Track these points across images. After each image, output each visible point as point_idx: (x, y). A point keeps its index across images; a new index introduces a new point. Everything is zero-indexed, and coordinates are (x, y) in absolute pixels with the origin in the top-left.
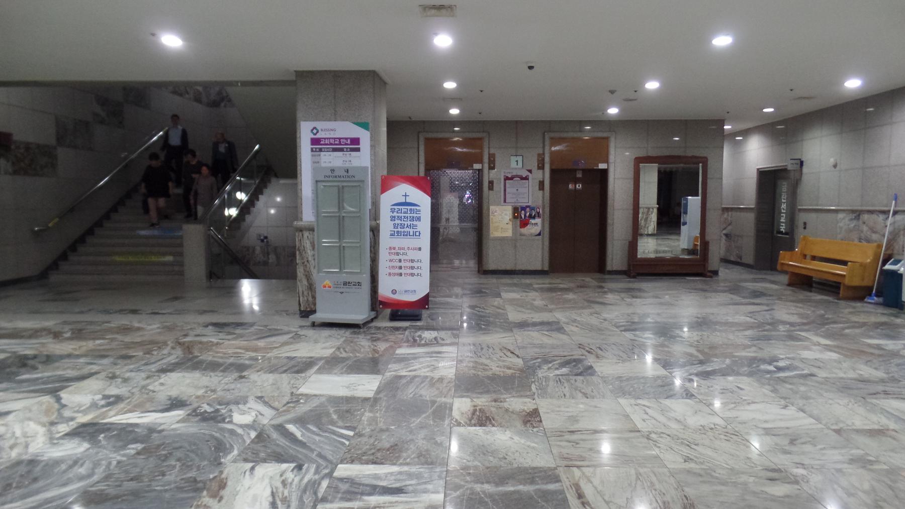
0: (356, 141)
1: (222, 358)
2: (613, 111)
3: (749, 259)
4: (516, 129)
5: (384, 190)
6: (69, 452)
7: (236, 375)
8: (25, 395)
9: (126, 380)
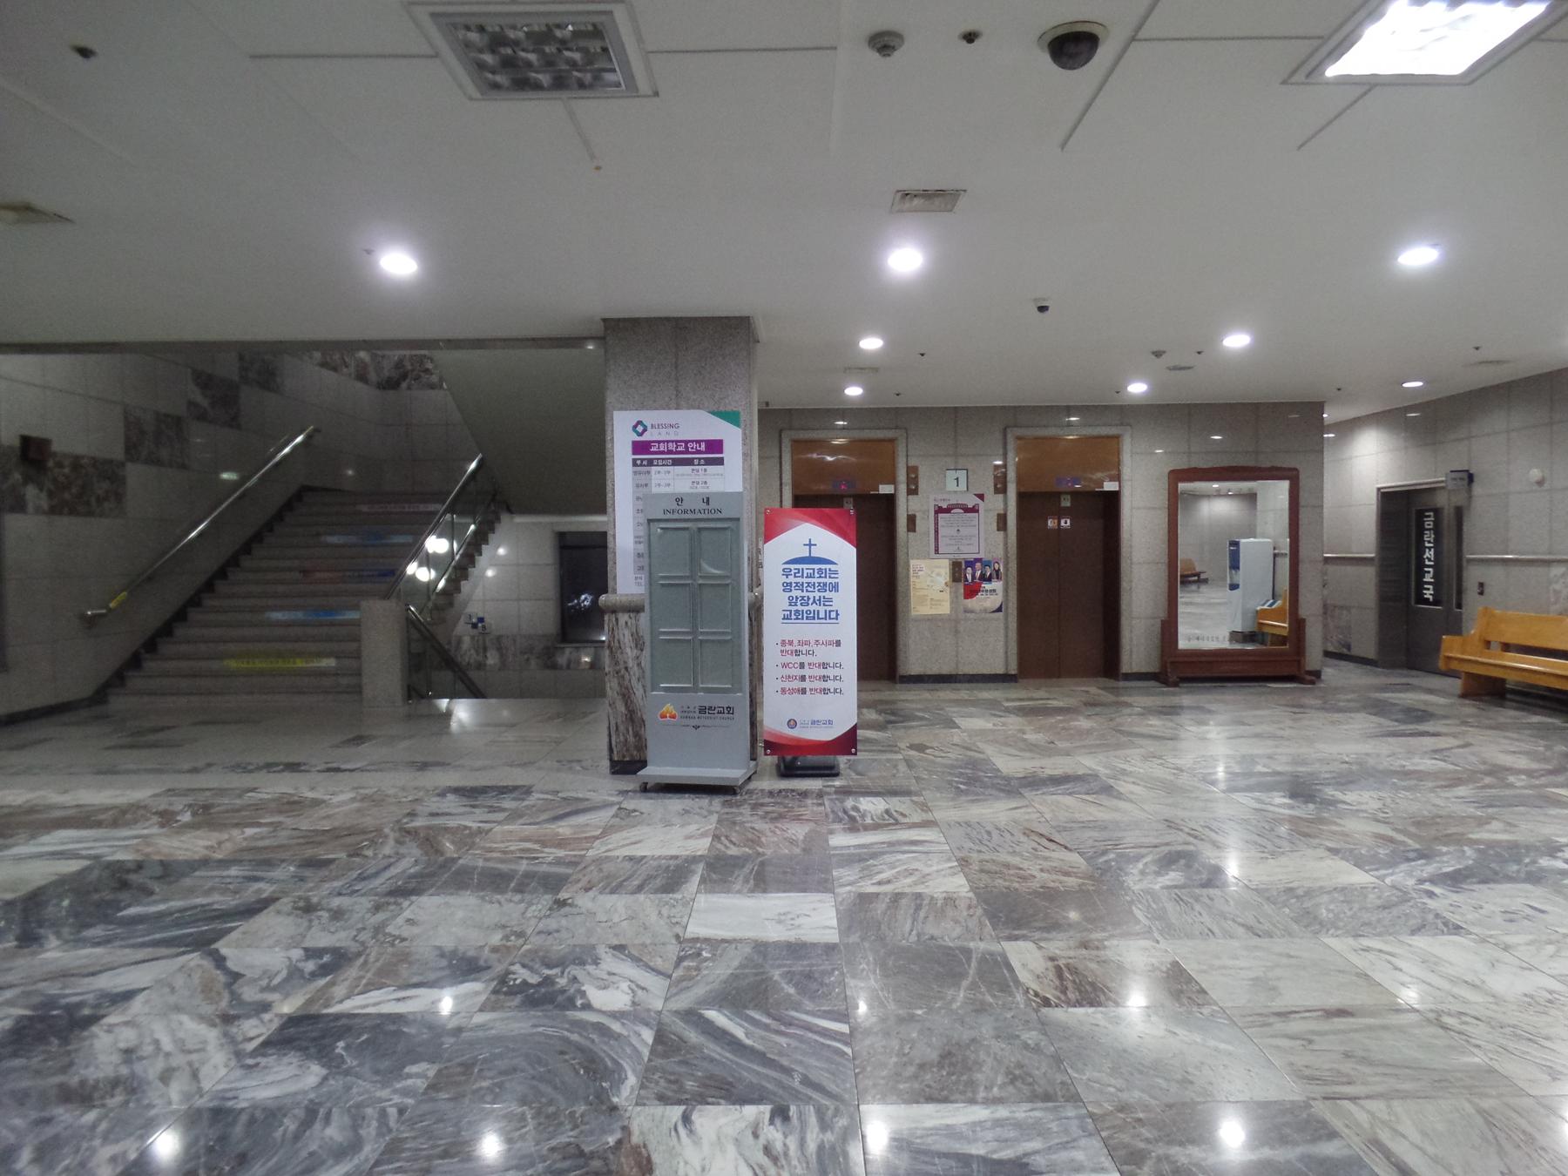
0: (715, 446)
1: (502, 861)
2: (1137, 388)
3: (1370, 651)
4: (956, 423)
5: (768, 538)
6: (290, 1088)
7: (547, 899)
8: (164, 951)
9: (337, 914)
